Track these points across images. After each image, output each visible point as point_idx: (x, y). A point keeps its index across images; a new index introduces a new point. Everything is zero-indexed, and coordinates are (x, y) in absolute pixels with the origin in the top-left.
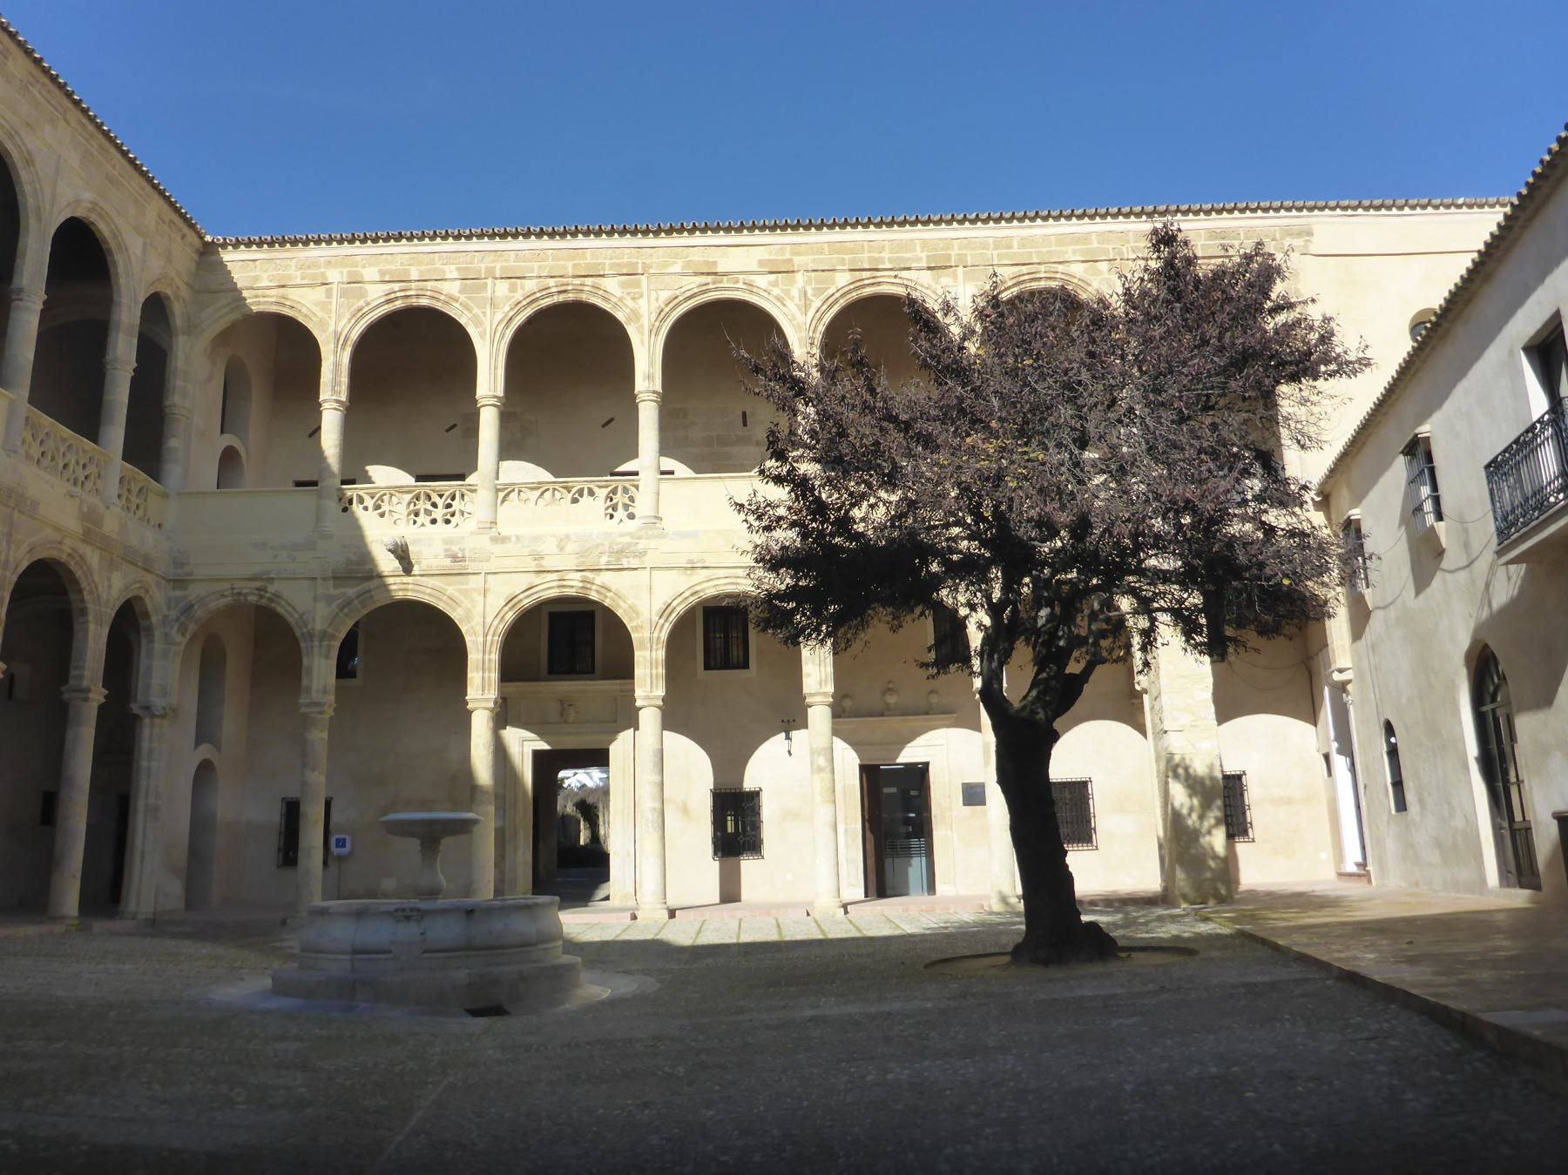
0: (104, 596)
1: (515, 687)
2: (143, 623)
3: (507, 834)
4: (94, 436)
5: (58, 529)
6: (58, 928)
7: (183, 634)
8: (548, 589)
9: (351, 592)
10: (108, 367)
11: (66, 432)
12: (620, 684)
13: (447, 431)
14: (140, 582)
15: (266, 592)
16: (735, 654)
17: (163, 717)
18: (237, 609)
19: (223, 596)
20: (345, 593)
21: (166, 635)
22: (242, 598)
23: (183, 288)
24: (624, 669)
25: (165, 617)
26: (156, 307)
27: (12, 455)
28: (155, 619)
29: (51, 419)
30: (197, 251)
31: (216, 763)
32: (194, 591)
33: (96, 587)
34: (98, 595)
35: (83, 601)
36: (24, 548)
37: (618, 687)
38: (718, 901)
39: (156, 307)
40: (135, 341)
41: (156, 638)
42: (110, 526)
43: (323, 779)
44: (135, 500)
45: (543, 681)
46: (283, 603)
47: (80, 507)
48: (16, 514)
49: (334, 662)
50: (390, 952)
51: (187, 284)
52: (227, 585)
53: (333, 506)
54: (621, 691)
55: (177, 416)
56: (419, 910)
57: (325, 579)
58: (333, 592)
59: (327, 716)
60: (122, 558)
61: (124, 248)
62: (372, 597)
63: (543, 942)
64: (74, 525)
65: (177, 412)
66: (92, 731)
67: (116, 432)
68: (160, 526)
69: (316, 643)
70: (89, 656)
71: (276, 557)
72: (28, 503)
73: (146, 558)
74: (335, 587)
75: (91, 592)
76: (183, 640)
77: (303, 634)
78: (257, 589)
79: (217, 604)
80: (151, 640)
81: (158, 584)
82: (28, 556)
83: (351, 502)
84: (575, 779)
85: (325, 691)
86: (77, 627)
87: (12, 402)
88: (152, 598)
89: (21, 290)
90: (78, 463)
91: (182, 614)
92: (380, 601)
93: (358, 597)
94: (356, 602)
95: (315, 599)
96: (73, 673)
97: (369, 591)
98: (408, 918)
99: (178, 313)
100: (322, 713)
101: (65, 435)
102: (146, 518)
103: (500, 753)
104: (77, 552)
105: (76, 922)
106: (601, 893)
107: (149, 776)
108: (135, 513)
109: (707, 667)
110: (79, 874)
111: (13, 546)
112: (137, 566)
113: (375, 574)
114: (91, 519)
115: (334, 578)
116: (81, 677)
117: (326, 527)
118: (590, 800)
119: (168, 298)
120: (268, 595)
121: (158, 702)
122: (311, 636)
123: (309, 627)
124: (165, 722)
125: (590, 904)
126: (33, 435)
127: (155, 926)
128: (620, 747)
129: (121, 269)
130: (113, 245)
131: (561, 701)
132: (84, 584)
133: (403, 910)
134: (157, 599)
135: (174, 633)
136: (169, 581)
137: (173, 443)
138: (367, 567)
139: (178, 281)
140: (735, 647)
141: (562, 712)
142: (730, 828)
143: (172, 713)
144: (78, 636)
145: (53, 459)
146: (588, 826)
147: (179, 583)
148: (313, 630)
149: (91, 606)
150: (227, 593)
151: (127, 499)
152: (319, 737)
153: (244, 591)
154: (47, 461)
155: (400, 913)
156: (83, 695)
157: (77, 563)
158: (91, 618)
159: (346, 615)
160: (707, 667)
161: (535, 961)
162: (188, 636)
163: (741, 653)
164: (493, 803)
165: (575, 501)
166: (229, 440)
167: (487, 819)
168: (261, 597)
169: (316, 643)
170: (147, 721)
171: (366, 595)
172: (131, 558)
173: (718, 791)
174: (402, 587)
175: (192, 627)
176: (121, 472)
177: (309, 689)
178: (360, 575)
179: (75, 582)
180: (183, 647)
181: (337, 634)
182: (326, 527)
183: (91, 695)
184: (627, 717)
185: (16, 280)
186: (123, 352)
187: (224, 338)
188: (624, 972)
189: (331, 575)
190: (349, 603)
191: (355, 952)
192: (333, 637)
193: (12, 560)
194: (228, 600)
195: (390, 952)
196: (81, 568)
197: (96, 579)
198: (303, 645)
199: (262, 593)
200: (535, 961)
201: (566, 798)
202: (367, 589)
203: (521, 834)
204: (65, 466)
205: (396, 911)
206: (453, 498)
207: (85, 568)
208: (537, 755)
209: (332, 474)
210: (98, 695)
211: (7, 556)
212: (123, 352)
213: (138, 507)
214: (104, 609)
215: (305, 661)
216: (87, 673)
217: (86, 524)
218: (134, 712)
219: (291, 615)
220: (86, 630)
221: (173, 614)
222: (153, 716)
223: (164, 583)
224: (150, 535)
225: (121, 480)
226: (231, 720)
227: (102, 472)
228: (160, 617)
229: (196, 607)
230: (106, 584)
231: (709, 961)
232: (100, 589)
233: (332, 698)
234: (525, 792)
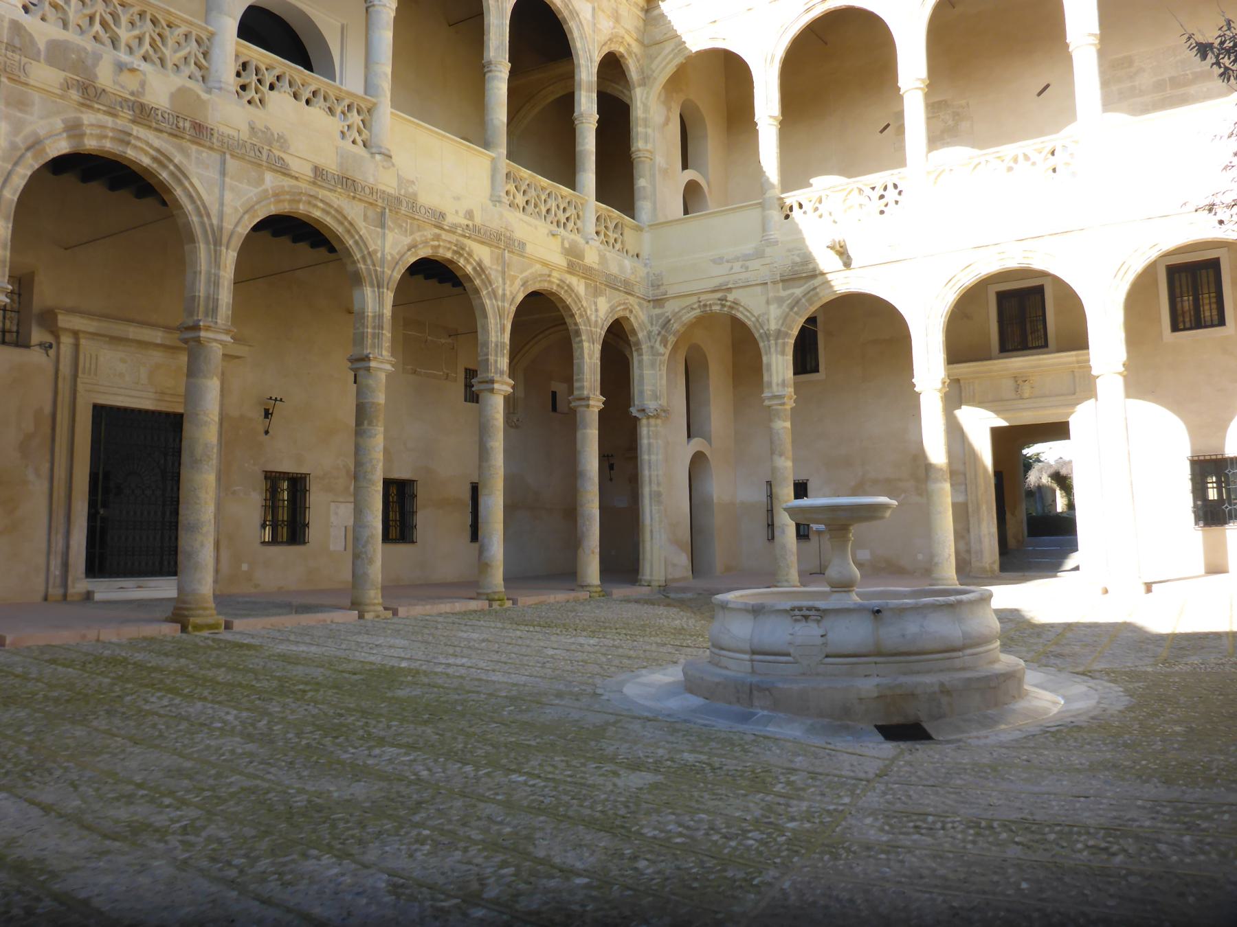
0: (593, 318)
1: (964, 369)
2: (632, 339)
3: (970, 510)
4: (572, 184)
5: (545, 264)
6: (582, 595)
7: (665, 346)
8: (989, 265)
9: (798, 291)
10: (576, 122)
11: (545, 182)
12: (1076, 356)
13: (882, 132)
14: (624, 303)
15: (727, 301)
16: (1207, 313)
17: (657, 417)
18: (706, 320)
19: (692, 309)
20: (793, 294)
21: (652, 347)
22: (708, 309)
23: (634, 45)
24: (1078, 340)
25: (650, 333)
26: (612, 66)
27: (498, 204)
28: (641, 335)
29: (530, 172)
30: (642, 9)
31: (707, 453)
32: (670, 307)
33: (585, 311)
34: (587, 318)
35: (576, 324)
36: (518, 283)
37: (1074, 359)
38: (1202, 571)
39: (612, 66)
40: (595, 96)
41: (644, 351)
42: (591, 258)
43: (789, 464)
44: (612, 236)
45: (995, 359)
46: (741, 309)
47: (563, 243)
48: (507, 254)
49: (790, 358)
50: (788, 655)
51: (637, 40)
52: (695, 299)
53: (776, 215)
54: (1078, 362)
55: (643, 159)
56: (817, 610)
57: (774, 283)
58: (783, 294)
59: (788, 407)
60: (605, 285)
61: (575, 15)
62: (817, 294)
63: (978, 645)
64: (560, 261)
65: (641, 155)
66: (596, 432)
67: (588, 178)
68: (637, 256)
69: (773, 342)
70: (586, 369)
71: (732, 268)
72: (516, 244)
73: (626, 283)
74: (784, 289)
75: (581, 316)
76: (665, 351)
77: (761, 336)
78: (719, 299)
79: (689, 316)
80: (639, 350)
81: (640, 305)
82: (522, 289)
83: (791, 209)
84: (1047, 452)
85: (784, 384)
86: (575, 346)
87: (493, 160)
88: (636, 317)
89: (490, 63)
90: (558, 206)
91: (662, 328)
92: (826, 297)
93: (804, 296)
94: (803, 300)
95: (768, 303)
96: (576, 385)
97: (815, 289)
98: (806, 617)
99: (633, 69)
100: (783, 404)
101: (545, 185)
102: (625, 250)
103: (955, 432)
104: (564, 282)
105: (599, 589)
106: (1070, 562)
107: (650, 467)
108: (613, 247)
109: (1175, 328)
110: (597, 550)
111: (508, 283)
112: (620, 291)
113: (817, 272)
114: (573, 254)
115: (783, 281)
116: (582, 388)
117: (771, 235)
118: (1063, 472)
119: (622, 56)
120: (728, 304)
121: (651, 405)
122: (767, 336)
123: (766, 328)
124: (659, 421)
125: (1059, 574)
126: (516, 187)
127: (667, 594)
128: (1080, 418)
129: (576, 34)
130: (566, 13)
131: (1015, 377)
132: (575, 309)
133: (800, 609)
134: (641, 319)
135: (657, 345)
136: (649, 301)
137: (641, 183)
138: (811, 266)
139: (628, 39)
140: (1207, 307)
141: (1017, 389)
142: (1212, 494)
143: (663, 414)
144: (576, 354)
145: (536, 206)
146: (1064, 494)
147: (658, 302)
148: (768, 330)
149: (582, 327)
150: (695, 306)
151: (605, 235)
152: (783, 426)
153: (708, 303)
154: (530, 208)
155: (797, 612)
156: (583, 403)
157: (566, 291)
158: (584, 338)
159: (796, 313)
160: (1175, 328)
161: (964, 669)
162: (670, 347)
163: (1215, 312)
164: (949, 480)
165: (1010, 169)
166: (690, 174)
167: (945, 496)
168: (723, 306)
169: (773, 342)
170: (644, 421)
171: (811, 294)
172: (613, 284)
173: (1196, 458)
174: (843, 282)
175: (672, 339)
176: (597, 211)
177: (770, 384)
178: (804, 275)
179: (568, 308)
180: (666, 357)
181: (789, 332)
182: (771, 235)
183: (591, 403)
184: (1083, 387)
185: (576, 109)
186: (587, 107)
187: (676, 81)
188: (1083, 674)
189: (779, 278)
190: (797, 302)
191: (754, 652)
192: (787, 335)
193: (508, 293)
194: (697, 312)
195: (788, 655)
196: (571, 296)
197: (585, 304)
198: (761, 345)
199: (724, 302)
200: (964, 669)
201: (1041, 471)
202: (812, 287)
203: (984, 508)
204: (548, 211)
205: (793, 609)
206: (885, 189)
207: (573, 296)
208: (997, 434)
209: (772, 186)
210: (597, 402)
211: (504, 290)
212: (587, 107)
213: (615, 240)
214: (593, 329)
215: (765, 359)
216: (586, 384)
217: (570, 258)
218: (634, 415)
219: (750, 320)
220: (582, 348)
221: (655, 329)
222: (648, 417)
223: (645, 304)
224: (627, 263)
225: (598, 219)
226: (718, 414)
227: (581, 213)
228: (645, 333)
229: (672, 322)
230: (593, 308)
231: (1195, 660)
232: (589, 312)
233: (791, 390)
234: (985, 469)
